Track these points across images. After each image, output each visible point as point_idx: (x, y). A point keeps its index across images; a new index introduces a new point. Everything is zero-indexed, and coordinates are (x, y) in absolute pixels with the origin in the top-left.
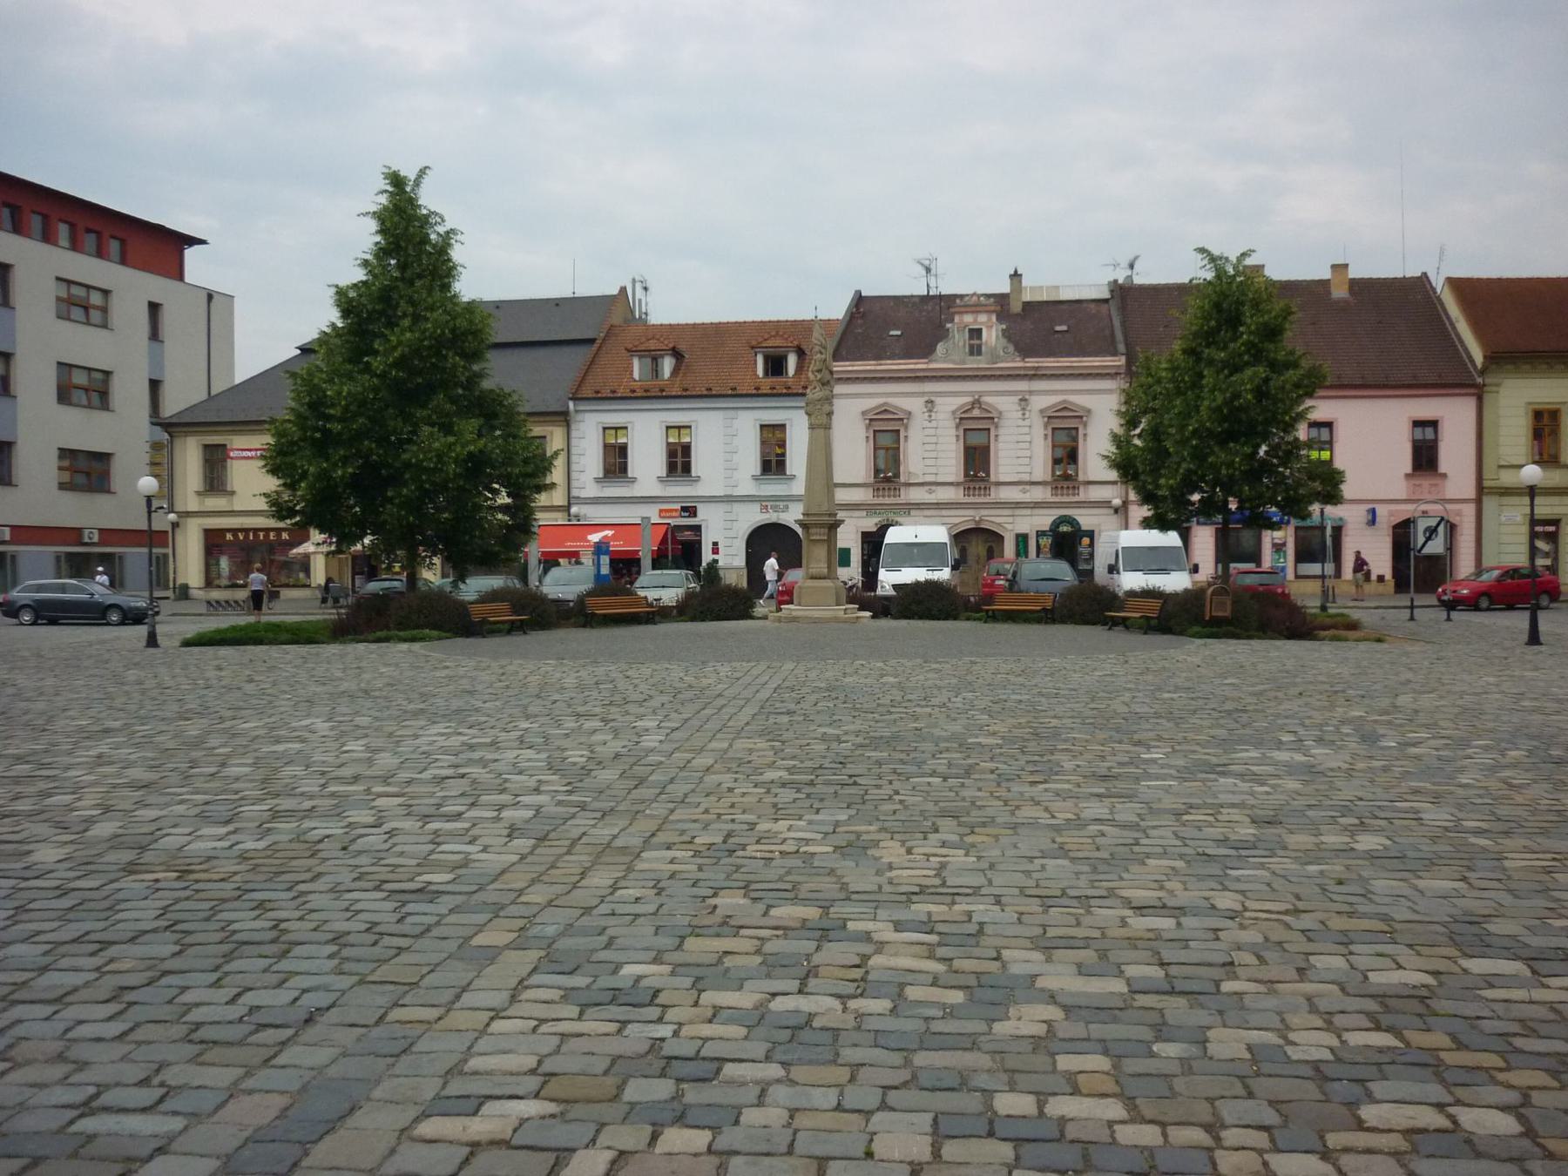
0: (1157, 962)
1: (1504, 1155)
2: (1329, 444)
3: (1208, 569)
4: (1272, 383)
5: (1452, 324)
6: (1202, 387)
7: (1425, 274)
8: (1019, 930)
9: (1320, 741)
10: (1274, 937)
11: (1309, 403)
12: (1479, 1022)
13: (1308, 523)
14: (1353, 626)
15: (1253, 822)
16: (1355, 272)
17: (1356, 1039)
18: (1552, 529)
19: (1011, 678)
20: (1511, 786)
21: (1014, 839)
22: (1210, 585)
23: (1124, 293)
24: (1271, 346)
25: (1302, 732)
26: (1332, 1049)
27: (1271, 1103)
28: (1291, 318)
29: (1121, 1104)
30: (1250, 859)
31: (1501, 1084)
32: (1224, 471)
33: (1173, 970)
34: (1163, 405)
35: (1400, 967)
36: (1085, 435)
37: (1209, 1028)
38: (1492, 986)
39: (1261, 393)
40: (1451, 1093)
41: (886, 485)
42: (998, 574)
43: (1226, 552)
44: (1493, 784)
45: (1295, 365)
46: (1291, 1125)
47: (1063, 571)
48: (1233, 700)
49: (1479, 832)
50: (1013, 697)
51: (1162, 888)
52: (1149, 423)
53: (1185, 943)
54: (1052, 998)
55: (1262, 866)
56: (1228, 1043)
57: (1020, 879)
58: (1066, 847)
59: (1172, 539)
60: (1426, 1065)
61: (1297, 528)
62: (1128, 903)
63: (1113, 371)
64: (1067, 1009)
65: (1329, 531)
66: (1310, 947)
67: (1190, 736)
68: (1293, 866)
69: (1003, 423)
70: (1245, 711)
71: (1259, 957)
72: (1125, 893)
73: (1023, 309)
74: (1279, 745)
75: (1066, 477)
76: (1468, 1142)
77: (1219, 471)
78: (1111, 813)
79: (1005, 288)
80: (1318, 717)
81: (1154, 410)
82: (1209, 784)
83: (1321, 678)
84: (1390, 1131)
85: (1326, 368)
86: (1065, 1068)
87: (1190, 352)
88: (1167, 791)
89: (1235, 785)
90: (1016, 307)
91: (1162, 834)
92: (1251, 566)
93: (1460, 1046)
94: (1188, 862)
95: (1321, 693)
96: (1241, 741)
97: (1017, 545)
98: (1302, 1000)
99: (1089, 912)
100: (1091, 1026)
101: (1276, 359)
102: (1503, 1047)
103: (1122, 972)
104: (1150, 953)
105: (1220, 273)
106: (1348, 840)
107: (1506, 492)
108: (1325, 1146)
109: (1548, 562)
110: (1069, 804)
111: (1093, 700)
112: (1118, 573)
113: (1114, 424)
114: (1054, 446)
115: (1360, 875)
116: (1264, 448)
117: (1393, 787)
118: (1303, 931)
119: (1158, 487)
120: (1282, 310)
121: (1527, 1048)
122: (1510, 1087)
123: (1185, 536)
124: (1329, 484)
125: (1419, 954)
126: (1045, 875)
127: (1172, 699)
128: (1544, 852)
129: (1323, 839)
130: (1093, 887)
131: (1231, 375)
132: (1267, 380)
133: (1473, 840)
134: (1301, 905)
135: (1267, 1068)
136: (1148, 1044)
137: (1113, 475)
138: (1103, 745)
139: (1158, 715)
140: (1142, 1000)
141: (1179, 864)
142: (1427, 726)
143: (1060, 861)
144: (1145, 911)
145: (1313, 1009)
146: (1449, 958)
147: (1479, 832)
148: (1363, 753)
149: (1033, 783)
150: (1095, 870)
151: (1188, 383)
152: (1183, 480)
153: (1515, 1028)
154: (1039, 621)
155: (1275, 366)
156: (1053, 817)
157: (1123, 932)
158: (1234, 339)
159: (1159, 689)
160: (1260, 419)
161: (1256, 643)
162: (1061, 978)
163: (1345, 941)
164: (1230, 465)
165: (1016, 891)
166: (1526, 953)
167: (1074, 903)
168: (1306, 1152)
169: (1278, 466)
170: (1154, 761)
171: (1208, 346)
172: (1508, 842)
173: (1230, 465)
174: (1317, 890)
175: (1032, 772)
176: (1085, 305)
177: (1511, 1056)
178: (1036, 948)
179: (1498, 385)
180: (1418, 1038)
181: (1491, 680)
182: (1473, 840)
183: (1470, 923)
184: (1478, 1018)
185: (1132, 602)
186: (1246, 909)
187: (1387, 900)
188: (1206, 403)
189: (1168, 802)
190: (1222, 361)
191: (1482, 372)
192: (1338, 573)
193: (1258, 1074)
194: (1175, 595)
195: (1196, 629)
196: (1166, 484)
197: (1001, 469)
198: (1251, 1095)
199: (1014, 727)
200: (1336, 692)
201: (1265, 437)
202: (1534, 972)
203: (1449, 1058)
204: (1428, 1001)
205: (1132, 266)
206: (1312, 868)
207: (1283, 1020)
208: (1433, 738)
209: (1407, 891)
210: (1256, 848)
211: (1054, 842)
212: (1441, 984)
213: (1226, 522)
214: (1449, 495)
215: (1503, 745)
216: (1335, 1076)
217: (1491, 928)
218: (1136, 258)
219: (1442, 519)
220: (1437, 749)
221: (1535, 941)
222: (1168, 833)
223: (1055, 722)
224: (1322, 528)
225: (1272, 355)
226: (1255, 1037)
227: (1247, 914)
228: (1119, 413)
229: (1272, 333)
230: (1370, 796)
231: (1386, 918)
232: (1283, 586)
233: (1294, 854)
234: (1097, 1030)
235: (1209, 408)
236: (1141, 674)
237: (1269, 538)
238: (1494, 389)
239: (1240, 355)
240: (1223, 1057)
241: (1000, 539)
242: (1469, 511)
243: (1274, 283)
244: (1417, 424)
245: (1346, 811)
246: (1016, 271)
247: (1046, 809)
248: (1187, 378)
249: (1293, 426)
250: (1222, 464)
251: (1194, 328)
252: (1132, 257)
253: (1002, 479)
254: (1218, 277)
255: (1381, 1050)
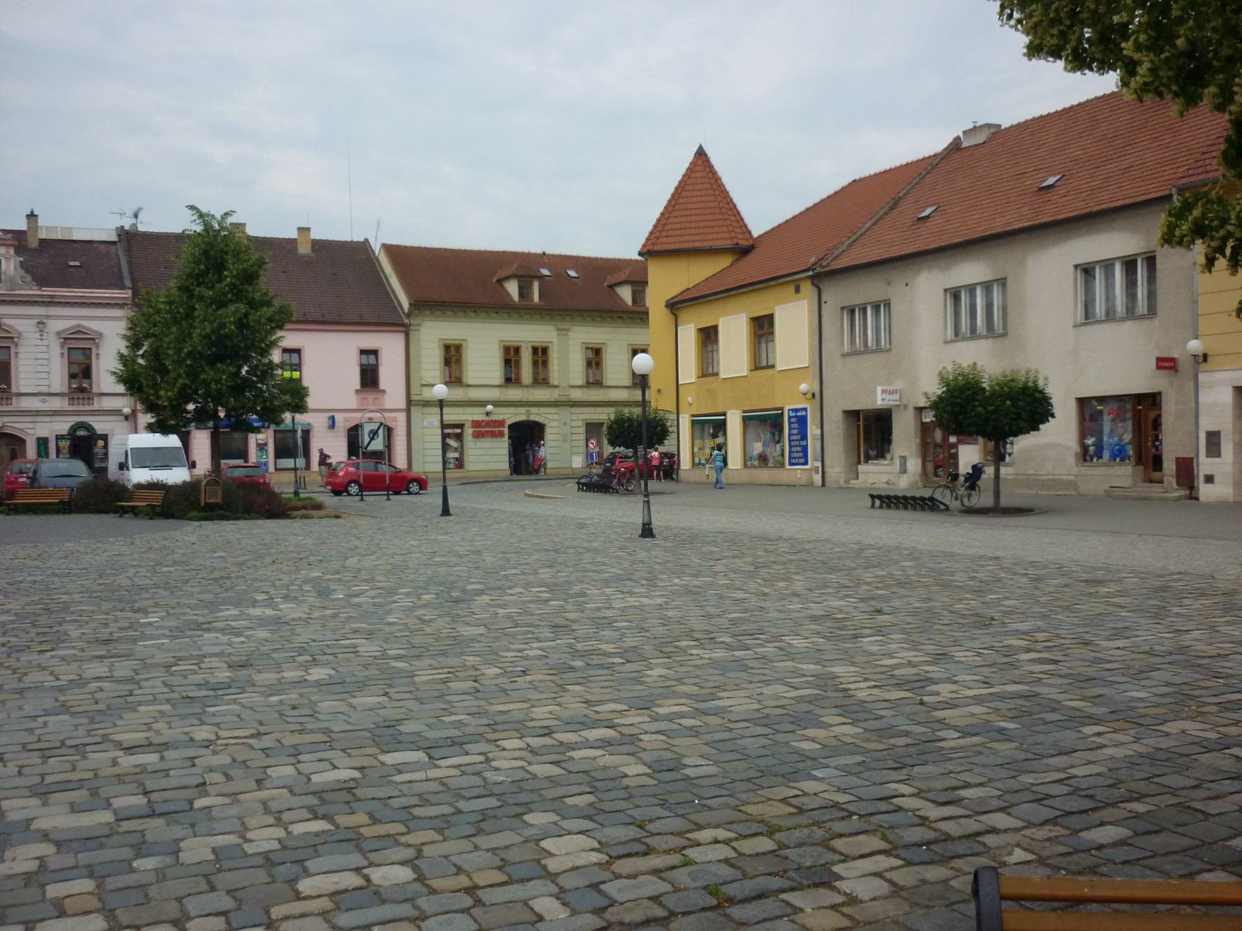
0: (139, 791)
1: (402, 898)
2: (298, 367)
3: (204, 463)
4: (251, 317)
5: (387, 279)
6: (193, 318)
7: (367, 240)
8: (18, 781)
9: (286, 598)
10: (240, 758)
11: (279, 333)
12: (391, 800)
13: (282, 427)
14: (318, 507)
15: (230, 666)
16: (316, 235)
17: (298, 829)
18: (459, 431)
19: (29, 562)
20: (423, 621)
21: (19, 703)
22: (205, 476)
23: (129, 238)
24: (250, 289)
25: (273, 592)
26: (280, 841)
27: (228, 892)
28: (265, 266)
29: (101, 917)
30: (226, 697)
31: (403, 845)
32: (213, 386)
33: (154, 797)
34: (162, 331)
35: (335, 767)
36: (98, 354)
37: (182, 840)
38: (400, 772)
39: (242, 324)
40: (366, 858)
41: (81, 396)
42: (21, 472)
43: (218, 452)
44: (411, 621)
45: (268, 304)
46: (244, 907)
47: (79, 469)
48: (220, 569)
49: (398, 658)
50: (28, 579)
51: (150, 729)
52: (150, 346)
53: (166, 772)
54: (45, 836)
55: (235, 702)
56: (197, 850)
57: (23, 737)
58: (69, 704)
59: (173, 441)
60: (349, 840)
61: (275, 432)
62: (119, 745)
63: (122, 302)
64: (58, 844)
65: (299, 434)
66: (268, 762)
67: (183, 601)
68: (260, 699)
69: (23, 342)
70: (229, 578)
71: (226, 775)
72: (117, 737)
73: (40, 246)
74: (254, 604)
75: (82, 390)
76: (376, 893)
77: (209, 385)
78: (111, 671)
79: (22, 225)
80: (286, 579)
81: (154, 335)
82: (195, 639)
83: (290, 549)
84: (319, 896)
85: (293, 307)
86: (54, 895)
87: (184, 289)
88: (159, 648)
89: (217, 638)
90: (33, 244)
91: (154, 684)
92: (240, 462)
93: (375, 821)
94: (173, 705)
95: (289, 560)
96: (224, 602)
97: (39, 448)
98: (259, 805)
99: (84, 758)
100: (79, 856)
101: (253, 299)
102: (406, 816)
103: (110, 805)
104: (135, 785)
105: (208, 227)
106: (303, 673)
107: (427, 404)
108: (269, 918)
109: (457, 455)
110: (74, 665)
111: (101, 576)
112: (128, 469)
113: (122, 346)
114: (70, 363)
115: (310, 700)
116: (245, 369)
117: (339, 629)
118: (263, 750)
119: (159, 397)
120: (257, 260)
121: (422, 815)
122: (409, 846)
123: (185, 440)
124: (296, 397)
125: (349, 755)
126: (47, 730)
127: (170, 572)
128: (442, 668)
129: (285, 674)
130: (89, 736)
131: (218, 309)
132: (246, 315)
133: (394, 664)
134: (262, 729)
135: (227, 864)
136: (129, 862)
137: (121, 388)
138: (106, 614)
139: (156, 586)
140: (126, 826)
141: (166, 708)
142: (366, 581)
143: (61, 717)
144: (134, 750)
145: (267, 811)
146: (371, 756)
147: (398, 658)
148: (319, 604)
149: (41, 652)
150: (92, 721)
151: (183, 315)
152: (179, 393)
153: (415, 801)
154: (57, 512)
155: (252, 304)
156: (58, 679)
157: (116, 770)
158: (220, 280)
159: (160, 564)
160: (242, 345)
161: (241, 523)
162: (57, 818)
163: (295, 753)
164: (218, 381)
165: (19, 748)
166: (425, 744)
167: (71, 751)
168: (255, 926)
169: (257, 382)
170: (150, 624)
171: (199, 285)
172: (419, 663)
173: (218, 381)
174: (277, 715)
175: (41, 643)
176: (96, 245)
177: (410, 821)
178: (35, 795)
179: (419, 325)
180: (345, 820)
181: (414, 543)
182: (394, 664)
183: (389, 727)
184: (390, 797)
185: (139, 493)
186: (218, 738)
187: (330, 717)
188: (198, 331)
189: (160, 658)
190: (211, 298)
191: (408, 315)
192: (308, 467)
193: (220, 871)
194: (175, 487)
195: (194, 513)
196: (165, 395)
197: (21, 382)
198: (213, 889)
199: (28, 604)
200: (301, 559)
201: (247, 359)
202: (430, 757)
203: (366, 832)
204: (354, 791)
205: (136, 216)
206: (274, 699)
207: (243, 823)
208: (372, 589)
209: (345, 709)
210: (230, 687)
211: (57, 701)
212: (364, 776)
213: (216, 428)
214: (387, 406)
215: (421, 591)
216: (281, 861)
217: (403, 729)
218: (140, 209)
219: (382, 424)
220: (372, 598)
221: (433, 735)
222: (158, 683)
223: (65, 598)
224: (295, 431)
225: (250, 295)
226: (220, 840)
227: (220, 742)
228: (125, 337)
229: (250, 277)
230: (322, 638)
231: (327, 731)
232: (264, 477)
233: (262, 689)
234: (84, 858)
235: (200, 335)
236: (146, 552)
237: (253, 439)
238: (417, 328)
239: (225, 294)
240: (193, 861)
241: (22, 442)
242: (402, 417)
243: (250, 238)
244: (363, 352)
245: (302, 651)
246: (32, 212)
247: (52, 673)
248: (181, 310)
249: (268, 352)
250: (212, 380)
251: (187, 270)
252: (136, 209)
253: (23, 390)
254: (206, 230)
255: (317, 834)
